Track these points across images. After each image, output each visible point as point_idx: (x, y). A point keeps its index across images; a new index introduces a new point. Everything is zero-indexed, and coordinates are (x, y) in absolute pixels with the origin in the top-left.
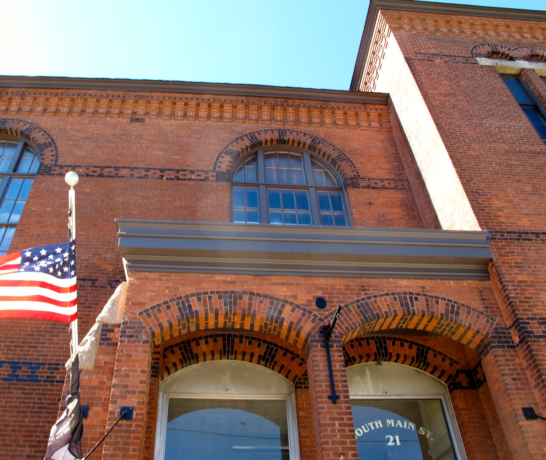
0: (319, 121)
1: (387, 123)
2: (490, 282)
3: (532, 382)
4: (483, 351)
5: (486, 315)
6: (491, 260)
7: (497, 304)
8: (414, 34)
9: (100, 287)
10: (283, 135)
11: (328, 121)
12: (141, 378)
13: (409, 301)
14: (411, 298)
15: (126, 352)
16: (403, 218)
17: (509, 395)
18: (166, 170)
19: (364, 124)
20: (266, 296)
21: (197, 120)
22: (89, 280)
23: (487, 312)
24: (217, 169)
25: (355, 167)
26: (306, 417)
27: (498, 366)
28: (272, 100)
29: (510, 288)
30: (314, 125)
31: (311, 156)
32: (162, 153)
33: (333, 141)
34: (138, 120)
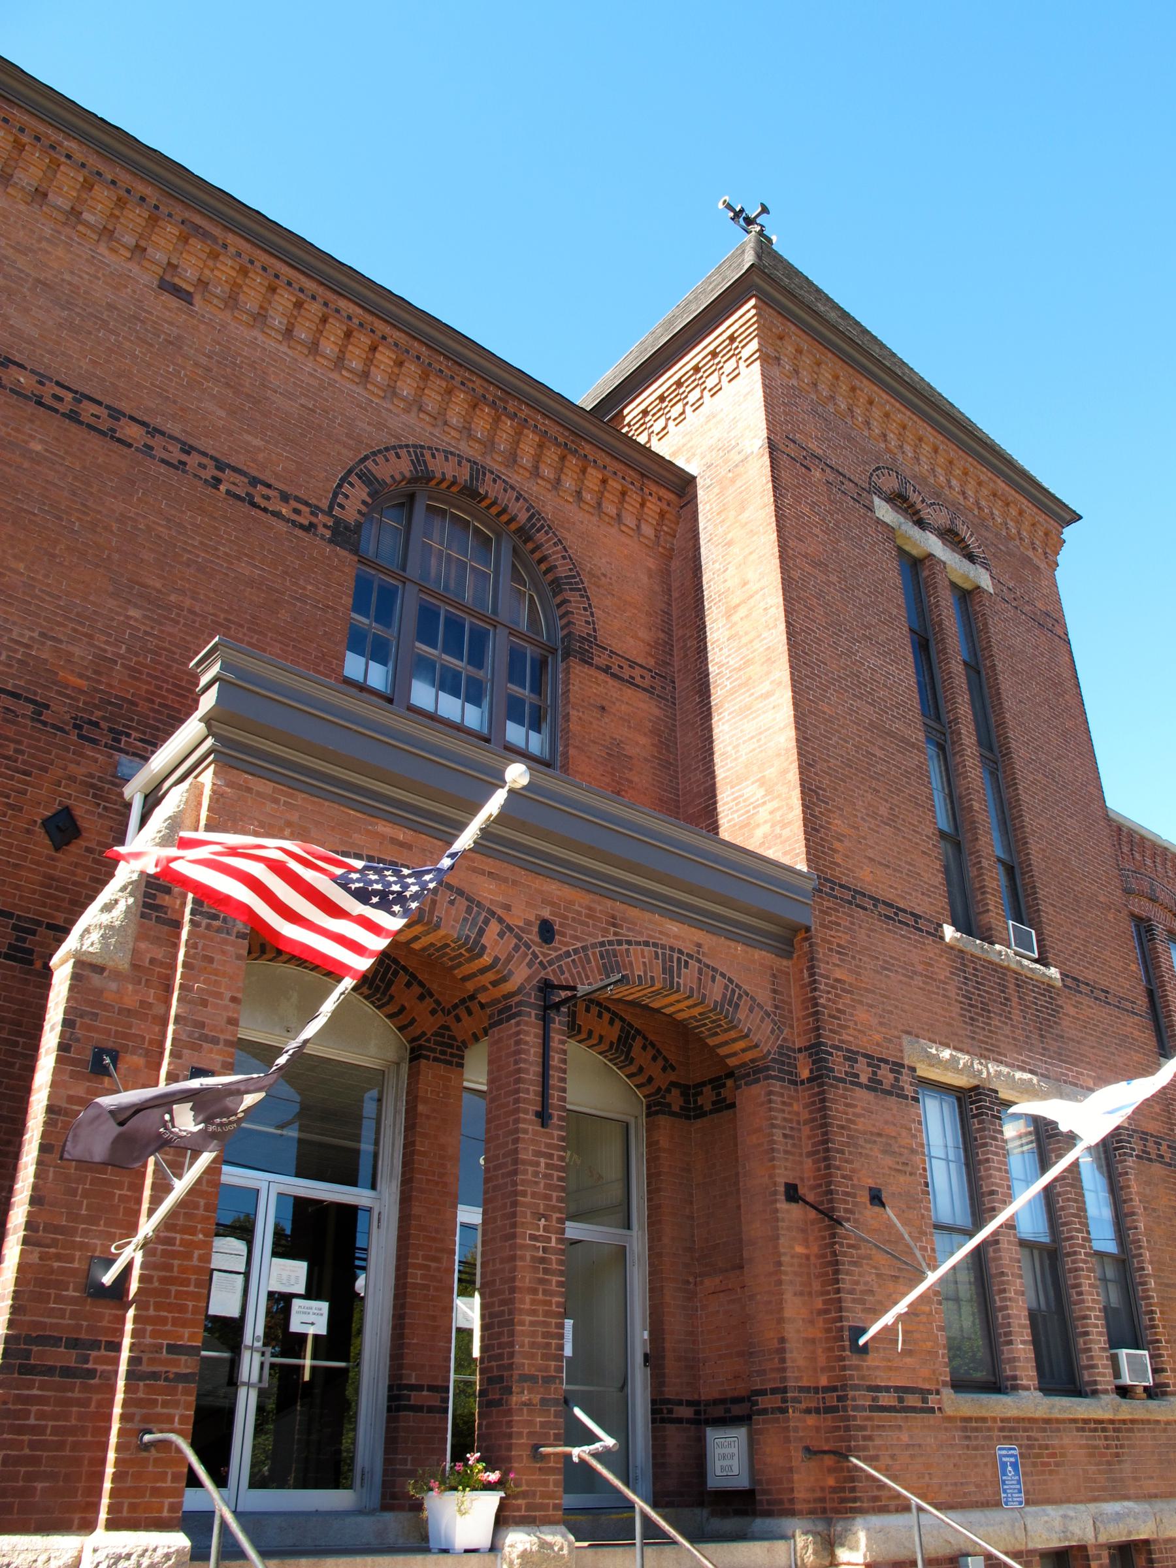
0: (552, 476)
1: (669, 538)
2: (790, 963)
3: (807, 1146)
4: (748, 1075)
5: (773, 1020)
6: (808, 929)
7: (790, 1004)
8: (793, 387)
9: (54, 726)
10: (477, 481)
11: (568, 483)
12: (230, 1014)
13: (675, 964)
14: (679, 959)
15: (203, 950)
16: (648, 761)
17: (773, 1159)
18: (229, 466)
19: (630, 521)
20: (460, 892)
21: (311, 358)
22: (27, 700)
23: (775, 1014)
24: (337, 511)
25: (592, 614)
26: (428, 1117)
27: (771, 1109)
28: (479, 382)
29: (822, 987)
30: (540, 481)
31: (515, 551)
32: (223, 414)
33: (567, 535)
34: (177, 291)
